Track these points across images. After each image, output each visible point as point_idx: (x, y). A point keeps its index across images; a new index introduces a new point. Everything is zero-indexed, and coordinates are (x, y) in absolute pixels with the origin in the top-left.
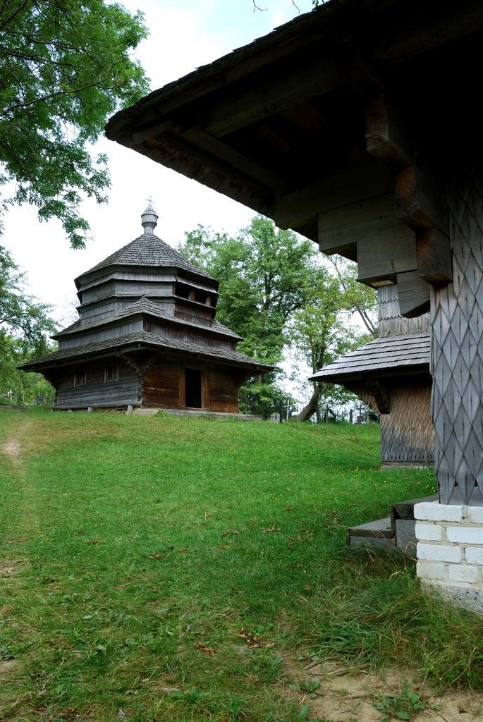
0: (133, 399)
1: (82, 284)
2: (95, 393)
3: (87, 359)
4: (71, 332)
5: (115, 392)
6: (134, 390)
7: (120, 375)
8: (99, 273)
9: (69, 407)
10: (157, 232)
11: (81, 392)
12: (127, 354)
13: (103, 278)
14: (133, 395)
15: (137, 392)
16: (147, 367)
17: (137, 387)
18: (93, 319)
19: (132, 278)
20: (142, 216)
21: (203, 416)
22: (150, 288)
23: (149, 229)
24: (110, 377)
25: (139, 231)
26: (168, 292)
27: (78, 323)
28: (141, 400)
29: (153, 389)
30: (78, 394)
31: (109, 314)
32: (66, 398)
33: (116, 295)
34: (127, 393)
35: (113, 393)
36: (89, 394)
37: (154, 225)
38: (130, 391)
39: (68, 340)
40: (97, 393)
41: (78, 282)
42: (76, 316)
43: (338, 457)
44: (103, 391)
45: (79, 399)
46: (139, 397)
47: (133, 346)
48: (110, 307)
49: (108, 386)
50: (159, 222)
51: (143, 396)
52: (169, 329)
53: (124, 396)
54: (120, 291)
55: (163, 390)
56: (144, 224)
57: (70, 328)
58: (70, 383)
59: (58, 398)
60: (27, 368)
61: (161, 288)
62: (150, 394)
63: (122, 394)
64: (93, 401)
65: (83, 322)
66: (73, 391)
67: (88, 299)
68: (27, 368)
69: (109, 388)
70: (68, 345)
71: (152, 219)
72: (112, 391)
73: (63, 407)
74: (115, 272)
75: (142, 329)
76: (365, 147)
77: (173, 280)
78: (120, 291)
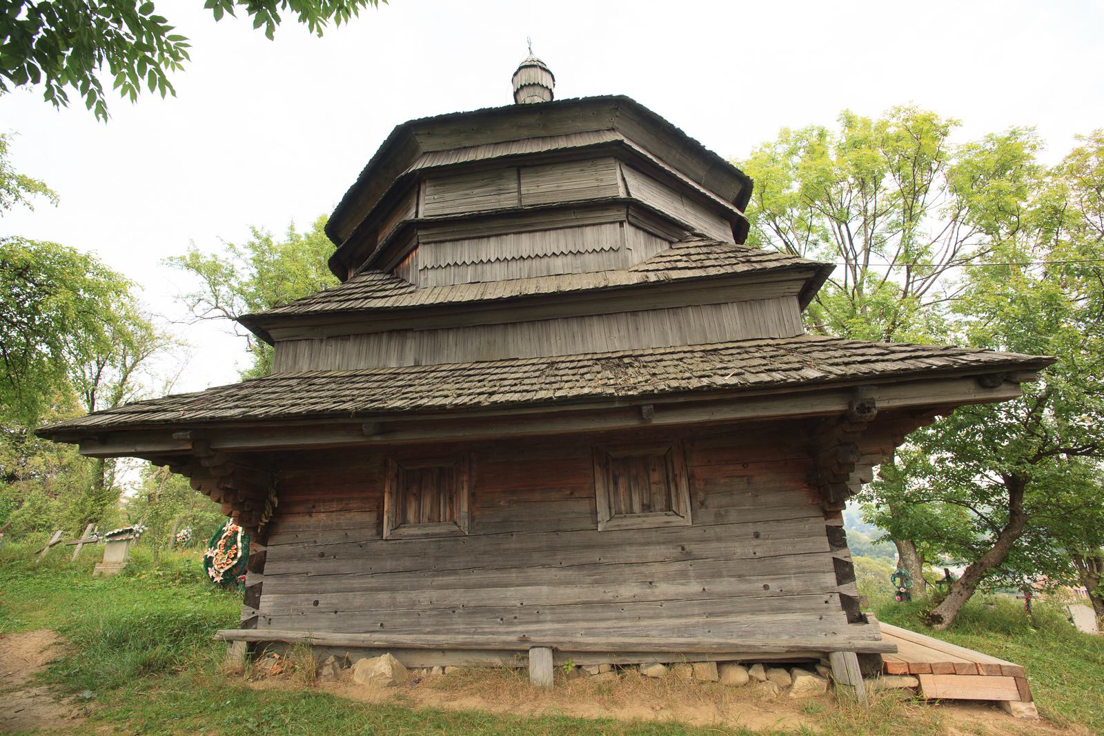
5: (683, 574)
9: (379, 639)
20: (520, 68)
32: (330, 583)
35: (668, 578)
38: (776, 573)
40: (552, 573)
44: (595, 565)
45: (426, 597)
69: (631, 554)
72: (657, 569)
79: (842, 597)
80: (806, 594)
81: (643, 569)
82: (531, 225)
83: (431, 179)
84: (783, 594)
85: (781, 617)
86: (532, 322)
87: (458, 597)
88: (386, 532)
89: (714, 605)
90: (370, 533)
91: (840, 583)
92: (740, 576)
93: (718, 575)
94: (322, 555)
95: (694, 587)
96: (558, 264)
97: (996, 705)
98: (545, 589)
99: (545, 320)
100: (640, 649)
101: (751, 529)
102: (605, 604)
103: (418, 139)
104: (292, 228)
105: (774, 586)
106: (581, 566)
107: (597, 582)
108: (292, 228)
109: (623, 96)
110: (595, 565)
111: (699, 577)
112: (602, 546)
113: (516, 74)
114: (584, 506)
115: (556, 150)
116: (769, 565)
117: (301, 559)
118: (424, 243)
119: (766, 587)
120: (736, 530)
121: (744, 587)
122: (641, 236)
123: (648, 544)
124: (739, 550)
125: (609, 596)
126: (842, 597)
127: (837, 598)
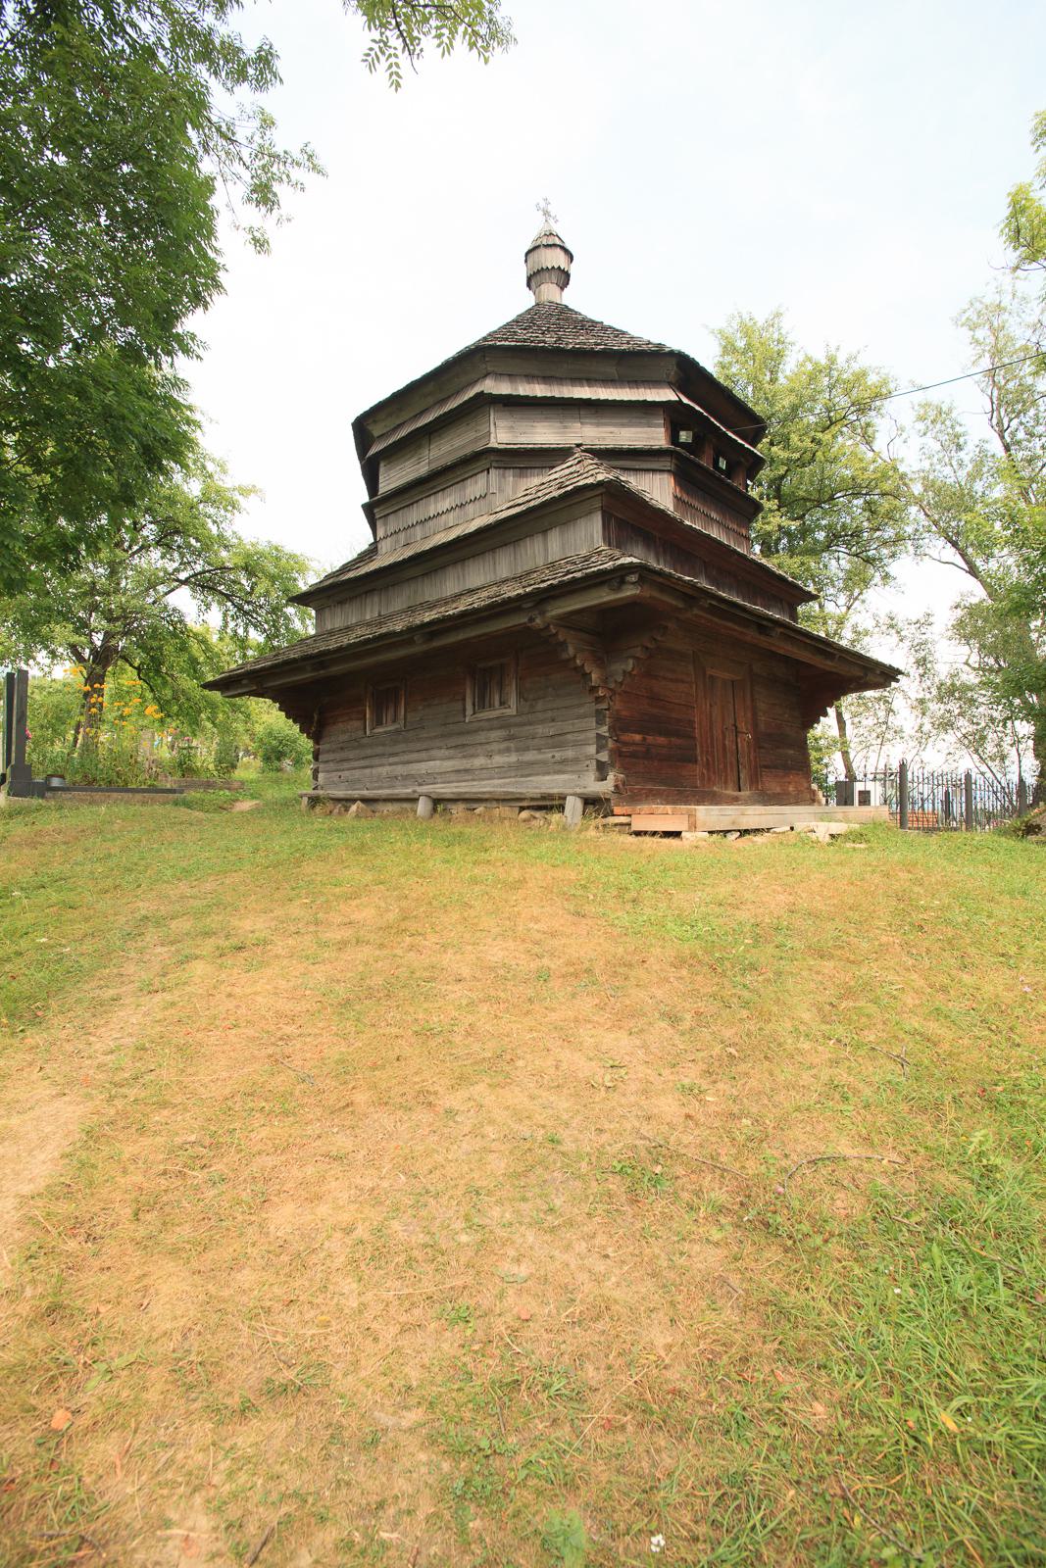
0: (579, 773)
1: (376, 433)
2: (434, 753)
3: (419, 647)
4: (351, 575)
5: (508, 750)
6: (576, 744)
7: (520, 695)
8: (431, 387)
9: (356, 794)
10: (574, 298)
11: (389, 750)
12: (566, 621)
13: (443, 401)
14: (576, 760)
15: (592, 749)
16: (630, 664)
17: (588, 737)
18: (419, 531)
19: (539, 390)
20: (527, 254)
21: (395, 813)
22: (598, 425)
23: (550, 292)
24: (482, 703)
25: (523, 301)
26: (655, 436)
27: (371, 552)
28: (611, 777)
29: (638, 737)
30: (383, 755)
31: (470, 508)
32: (346, 765)
33: (493, 444)
34: (548, 755)
35: (500, 752)
36: (415, 756)
37: (563, 278)
38: (560, 746)
39: (341, 603)
40: (444, 752)
41: (363, 428)
42: (360, 536)
43: (457, 851)
44: (464, 745)
45: (384, 770)
46: (602, 770)
47: (602, 583)
48: (475, 487)
49: (476, 731)
50: (573, 270)
51: (612, 765)
52: (665, 552)
53: (544, 762)
54: (503, 433)
55: (662, 740)
56: (533, 279)
57: (345, 568)
58: (357, 724)
59: (321, 766)
60: (233, 684)
61: (623, 425)
62: (633, 755)
63: (531, 756)
64: (431, 777)
65: (384, 547)
66: (362, 746)
67: (392, 479)
68: (233, 684)
69: (481, 737)
70: (337, 620)
71: (556, 259)
72: (495, 747)
73: (340, 793)
74: (485, 376)
75: (599, 542)
76: (683, 430)
77: (667, 395)
78: (503, 433)
79: (598, 761)
80: (576, 760)
81: (487, 746)
82: (432, 488)
83: (384, 459)
84: (563, 762)
85: (556, 777)
86: (455, 563)
87: (400, 770)
88: (368, 732)
89: (524, 769)
90: (360, 733)
91: (598, 752)
92: (539, 749)
93: (527, 749)
94: (342, 749)
95: (513, 758)
96: (451, 519)
97: (677, 834)
98: (438, 762)
99: (463, 560)
100: (467, 796)
101: (549, 714)
102: (466, 771)
103: (370, 428)
104: (778, 315)
105: (558, 755)
106: (456, 747)
107: (464, 757)
108: (778, 315)
109: (353, 425)
110: (464, 745)
111: (517, 750)
112: (468, 733)
113: (526, 261)
114: (458, 706)
115: (465, 402)
116: (557, 741)
117: (334, 751)
118: (496, 468)
119: (553, 757)
120: (540, 716)
121: (540, 757)
122: (737, 392)
123: (491, 729)
124: (540, 731)
125: (468, 766)
126: (598, 761)
127: (594, 763)
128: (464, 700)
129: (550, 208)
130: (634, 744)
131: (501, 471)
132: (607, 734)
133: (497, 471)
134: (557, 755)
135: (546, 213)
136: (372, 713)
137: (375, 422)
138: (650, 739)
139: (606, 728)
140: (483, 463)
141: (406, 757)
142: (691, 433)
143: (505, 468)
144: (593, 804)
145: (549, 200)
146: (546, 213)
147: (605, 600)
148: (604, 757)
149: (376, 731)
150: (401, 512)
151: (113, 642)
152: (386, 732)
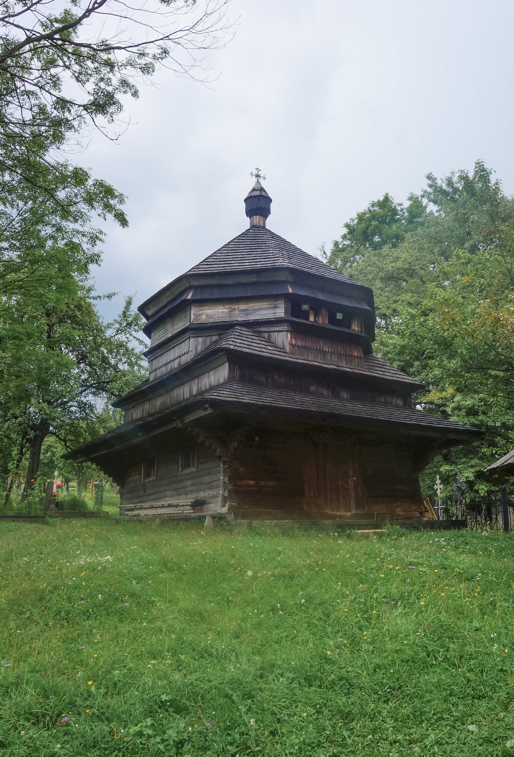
24: (187, 465)
29: (252, 482)
38: (210, 488)
44: (177, 489)
72: (189, 489)
109: (270, 213)
118: (193, 337)
128: (178, 463)
129: (260, 173)
130: (249, 486)
131: (196, 339)
132: (227, 482)
133: (194, 339)
134: (210, 493)
135: (258, 176)
136: (144, 471)
137: (148, 309)
138: (262, 483)
139: (227, 478)
140: (187, 335)
141: (155, 496)
142: (308, 305)
143: (197, 337)
144: (218, 518)
145: (260, 168)
146: (258, 176)
147: (202, 414)
148: (226, 495)
149: (146, 481)
150: (158, 359)
151: (324, 312)
152: (149, 482)
